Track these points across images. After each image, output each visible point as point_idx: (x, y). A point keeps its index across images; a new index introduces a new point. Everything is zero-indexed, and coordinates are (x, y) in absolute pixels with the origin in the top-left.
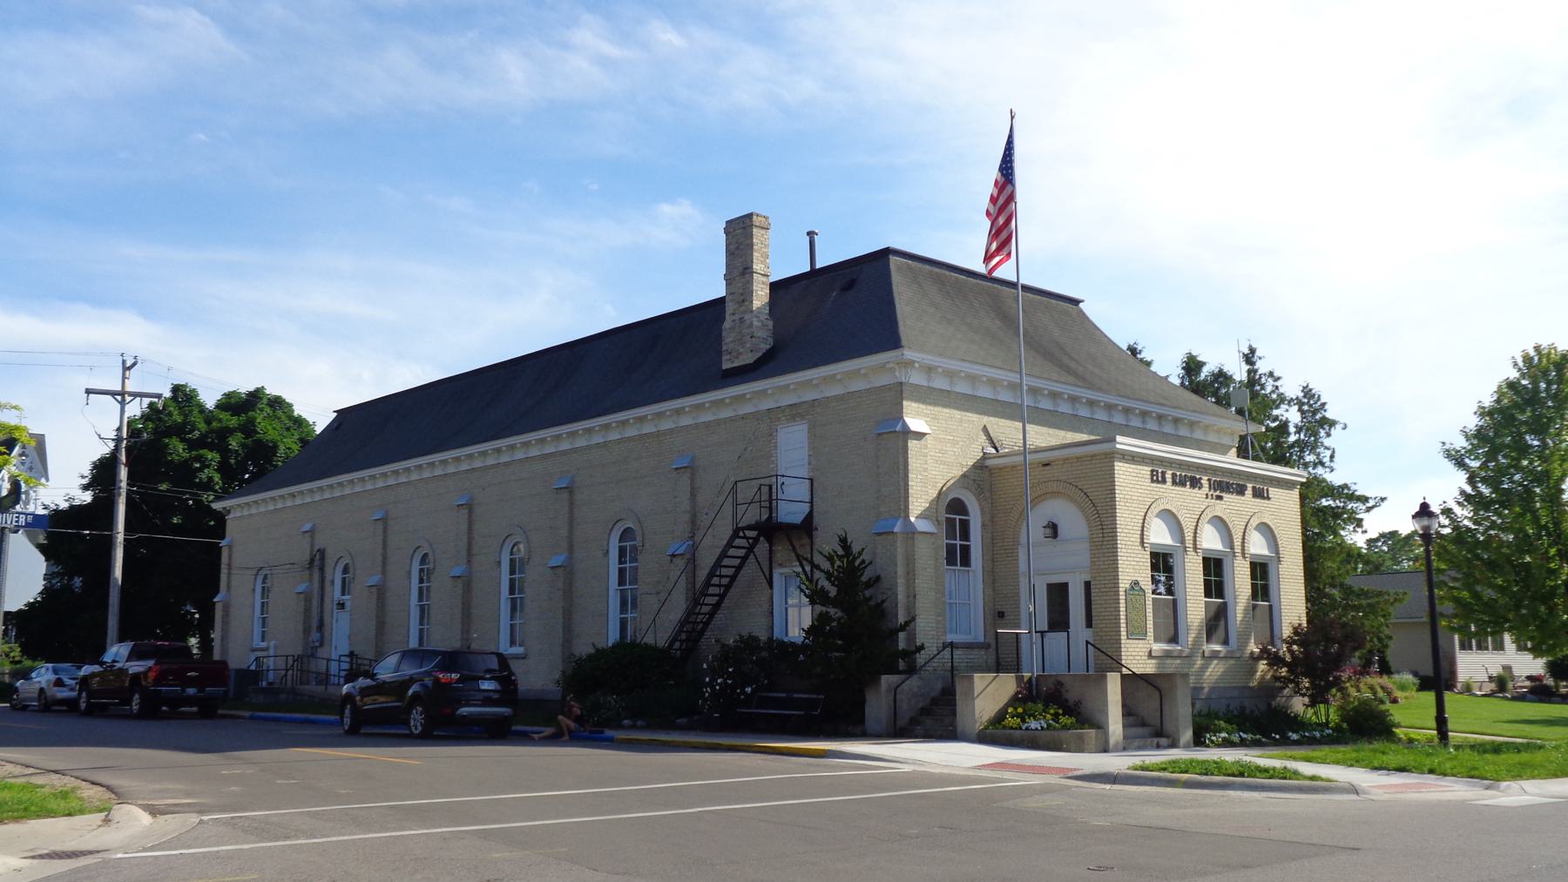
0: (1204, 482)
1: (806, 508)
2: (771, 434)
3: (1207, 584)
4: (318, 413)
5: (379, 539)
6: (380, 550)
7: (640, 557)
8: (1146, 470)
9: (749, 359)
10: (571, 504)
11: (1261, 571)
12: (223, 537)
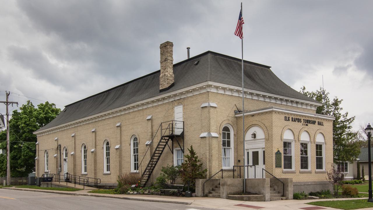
0: (302, 121)
1: (182, 130)
2: (173, 108)
3: (317, 152)
4: (61, 106)
5: (73, 142)
6: (74, 145)
7: (139, 146)
8: (283, 117)
9: (167, 86)
10: (121, 130)
11: (319, 147)
12: (36, 142)
